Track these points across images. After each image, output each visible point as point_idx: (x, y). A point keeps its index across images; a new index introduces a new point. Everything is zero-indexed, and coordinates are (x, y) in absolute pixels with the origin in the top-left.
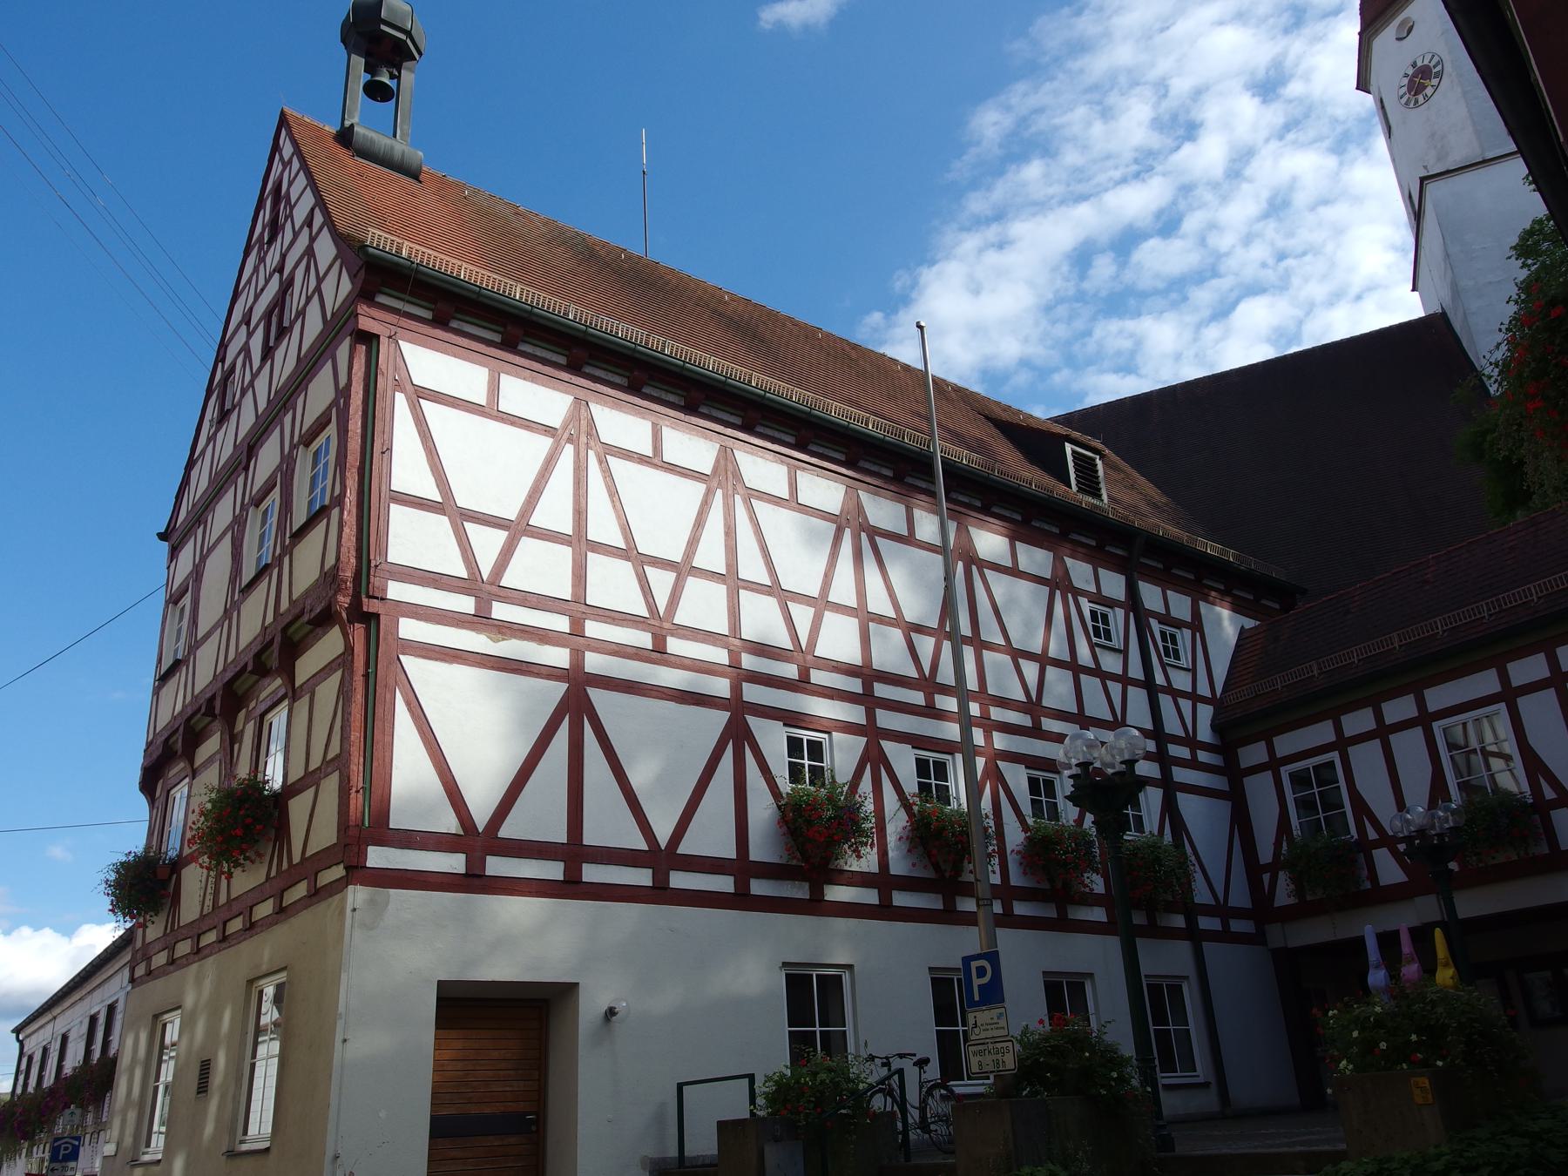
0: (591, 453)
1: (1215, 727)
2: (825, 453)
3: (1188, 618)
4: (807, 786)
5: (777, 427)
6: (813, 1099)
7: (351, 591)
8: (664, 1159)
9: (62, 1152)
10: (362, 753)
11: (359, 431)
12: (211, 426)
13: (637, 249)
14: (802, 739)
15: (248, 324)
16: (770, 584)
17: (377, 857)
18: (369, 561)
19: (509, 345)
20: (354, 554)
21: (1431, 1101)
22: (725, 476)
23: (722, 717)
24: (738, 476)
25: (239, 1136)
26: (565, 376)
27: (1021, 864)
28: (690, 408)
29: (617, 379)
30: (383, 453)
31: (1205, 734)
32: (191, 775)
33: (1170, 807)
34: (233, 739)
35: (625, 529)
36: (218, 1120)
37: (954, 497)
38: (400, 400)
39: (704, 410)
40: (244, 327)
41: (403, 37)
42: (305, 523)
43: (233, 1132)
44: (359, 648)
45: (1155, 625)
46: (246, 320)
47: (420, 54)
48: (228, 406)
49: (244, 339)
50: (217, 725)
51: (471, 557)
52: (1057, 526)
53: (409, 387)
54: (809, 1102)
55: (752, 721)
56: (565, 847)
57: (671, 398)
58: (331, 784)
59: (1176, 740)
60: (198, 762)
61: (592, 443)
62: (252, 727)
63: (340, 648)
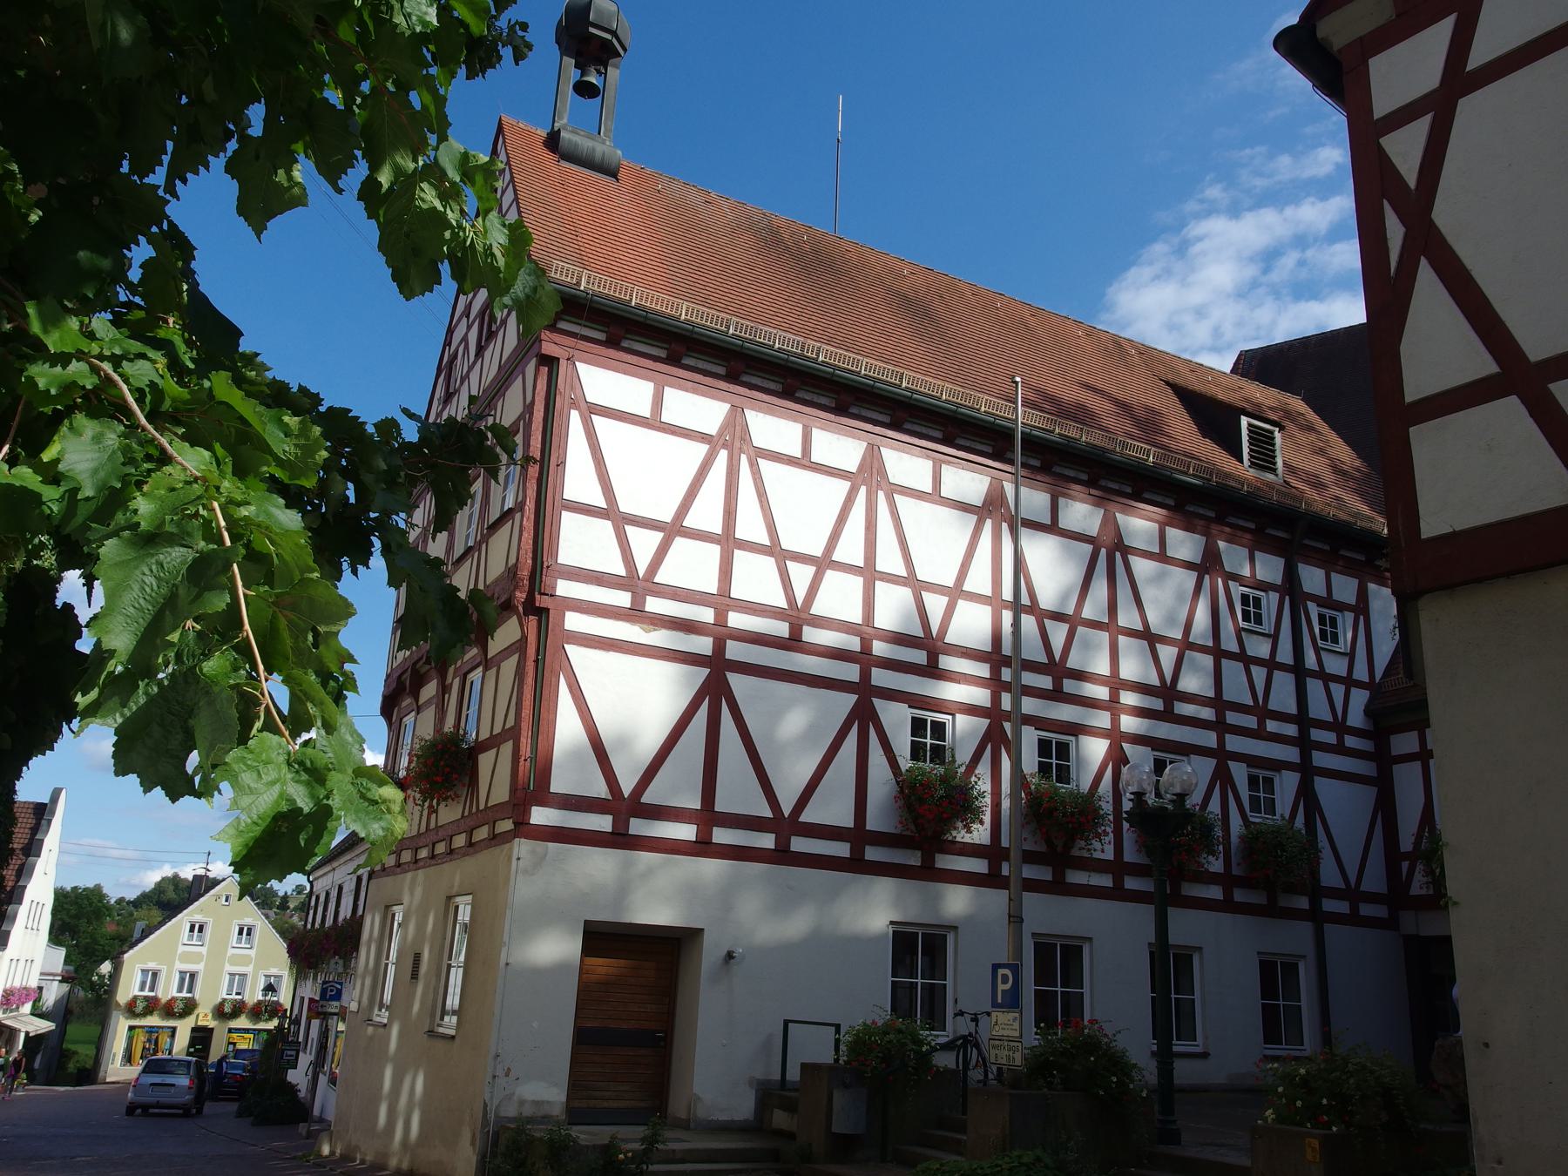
0: (744, 458)
1: (1368, 712)
2: (973, 446)
3: (1352, 600)
4: (927, 766)
5: (926, 424)
6: (880, 1055)
7: (527, 588)
8: (769, 1081)
9: (329, 993)
10: (530, 728)
11: (539, 446)
12: (439, 404)
13: (823, 227)
14: (926, 720)
15: (468, 317)
16: (906, 576)
17: (540, 816)
18: (543, 562)
19: (673, 360)
20: (531, 555)
21: (1318, 1160)
22: (870, 474)
23: (850, 699)
24: (882, 472)
25: (437, 1020)
26: (723, 385)
27: (1137, 841)
28: (841, 410)
29: (772, 386)
30: (558, 465)
31: (1356, 718)
32: (416, 709)
33: (1306, 793)
34: (444, 689)
35: (770, 527)
36: (422, 1003)
37: (1103, 484)
38: (575, 416)
39: (854, 410)
40: (465, 319)
41: (608, 36)
42: (499, 518)
43: (433, 1015)
44: (532, 638)
45: (1314, 609)
46: (467, 313)
47: (625, 50)
48: (451, 390)
49: (465, 330)
50: (433, 673)
51: (630, 557)
52: (1213, 510)
53: (583, 405)
54: (878, 1057)
55: (877, 702)
56: (699, 812)
57: (823, 401)
58: (507, 748)
59: (1321, 725)
60: (422, 700)
61: (745, 448)
62: (458, 683)
63: (518, 636)
